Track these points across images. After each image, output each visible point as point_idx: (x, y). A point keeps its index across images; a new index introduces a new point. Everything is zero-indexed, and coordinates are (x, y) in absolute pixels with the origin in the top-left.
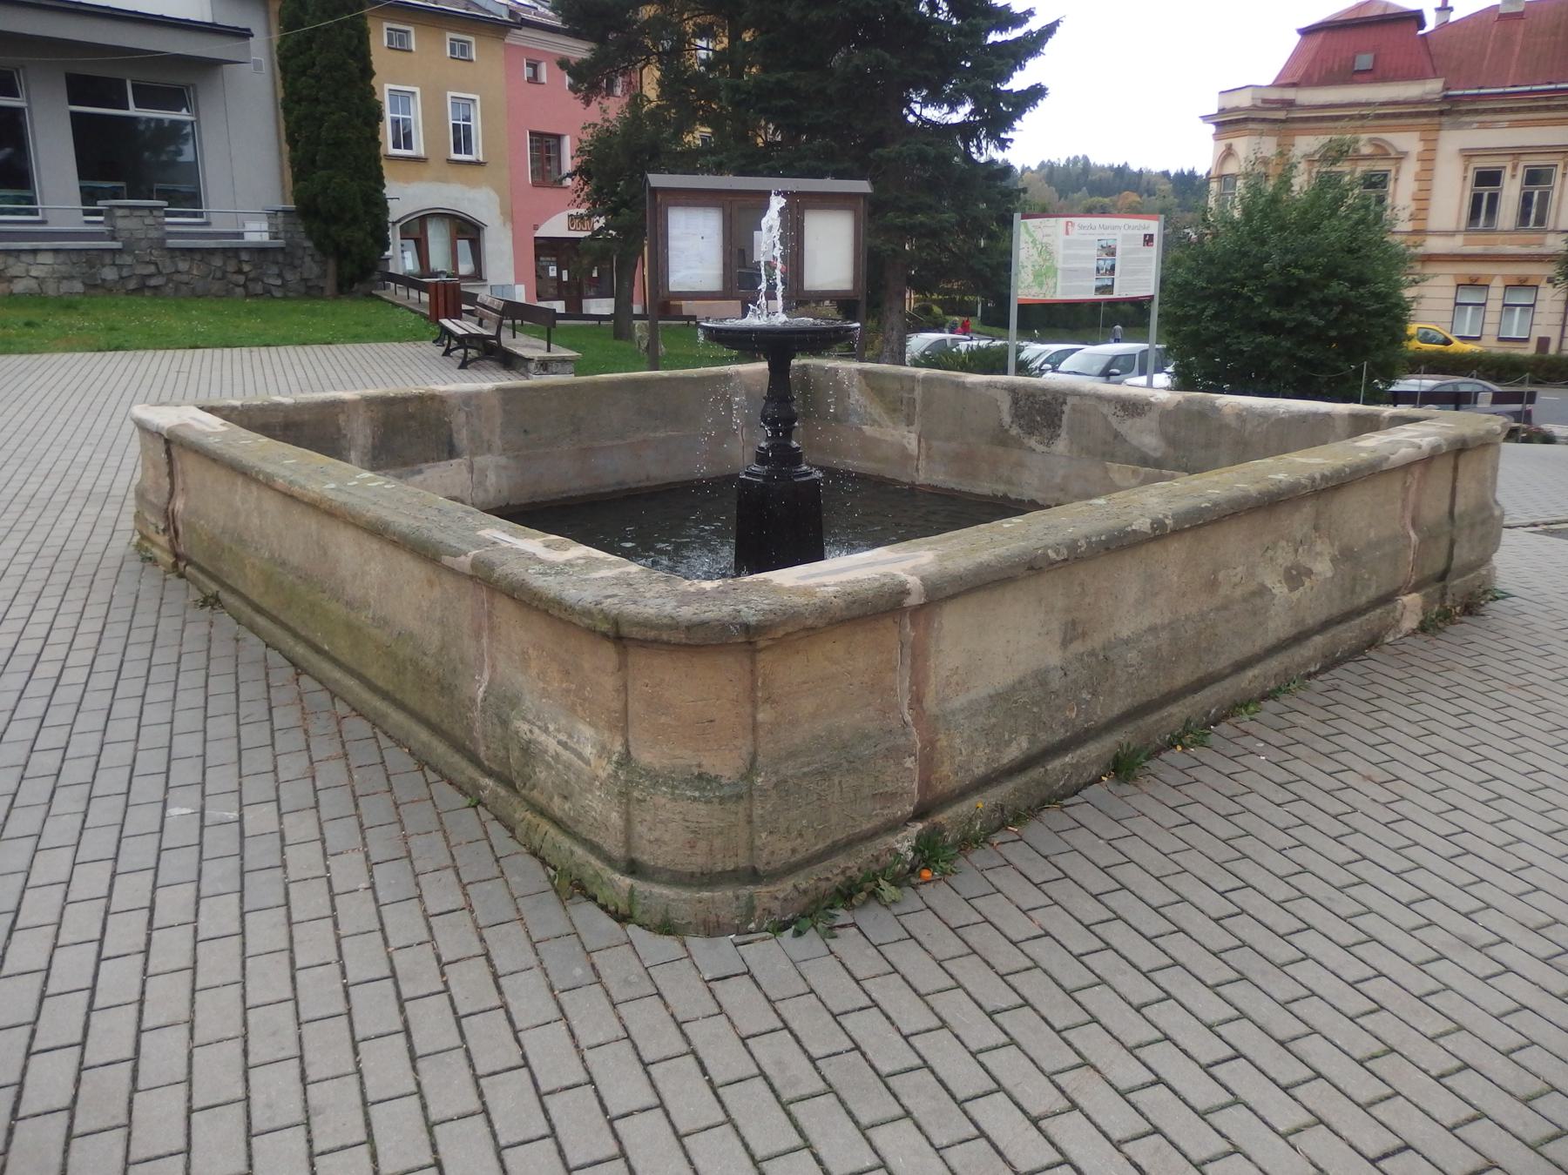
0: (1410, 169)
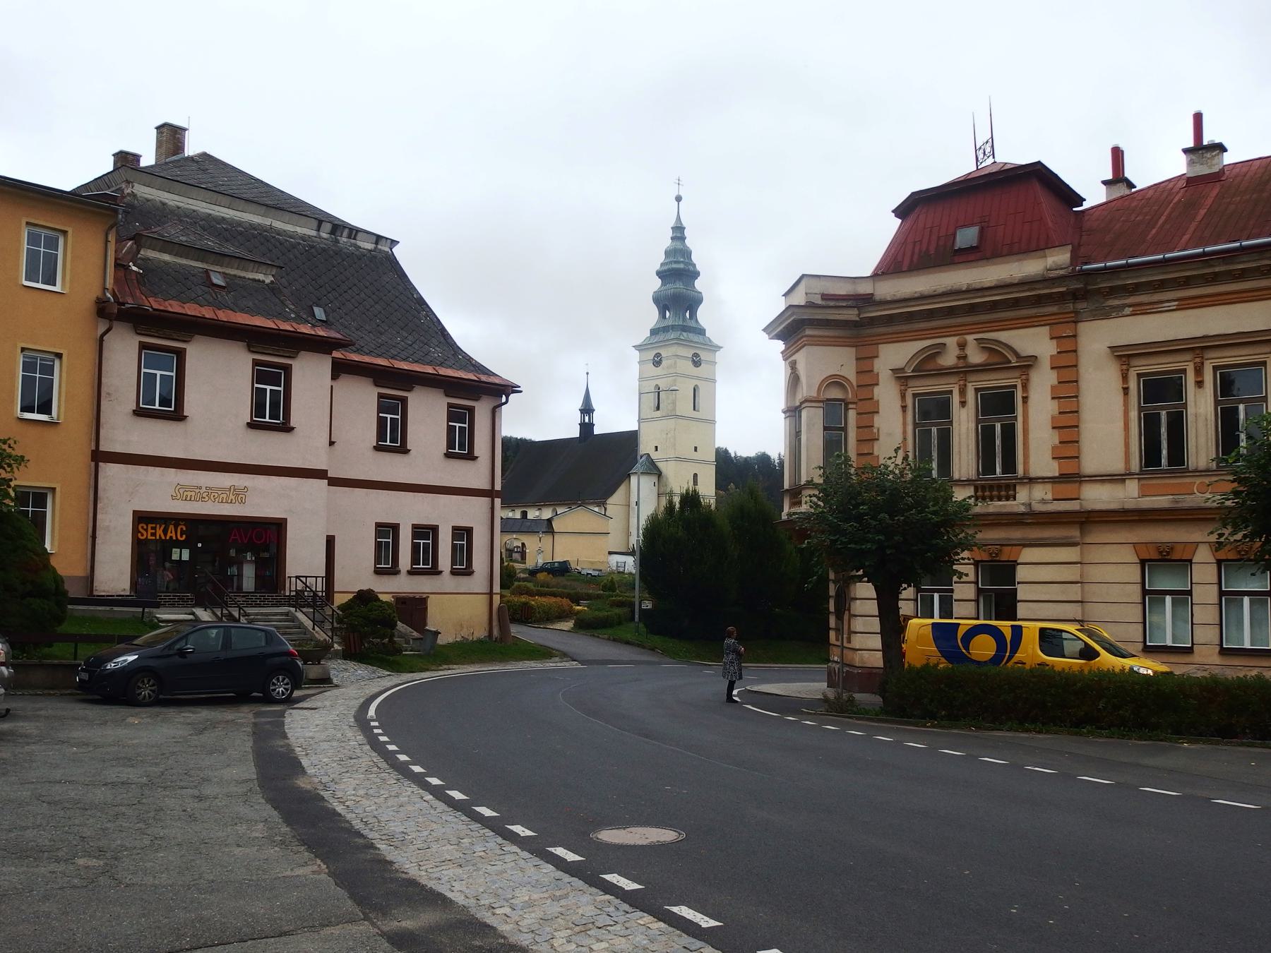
0: (1043, 382)
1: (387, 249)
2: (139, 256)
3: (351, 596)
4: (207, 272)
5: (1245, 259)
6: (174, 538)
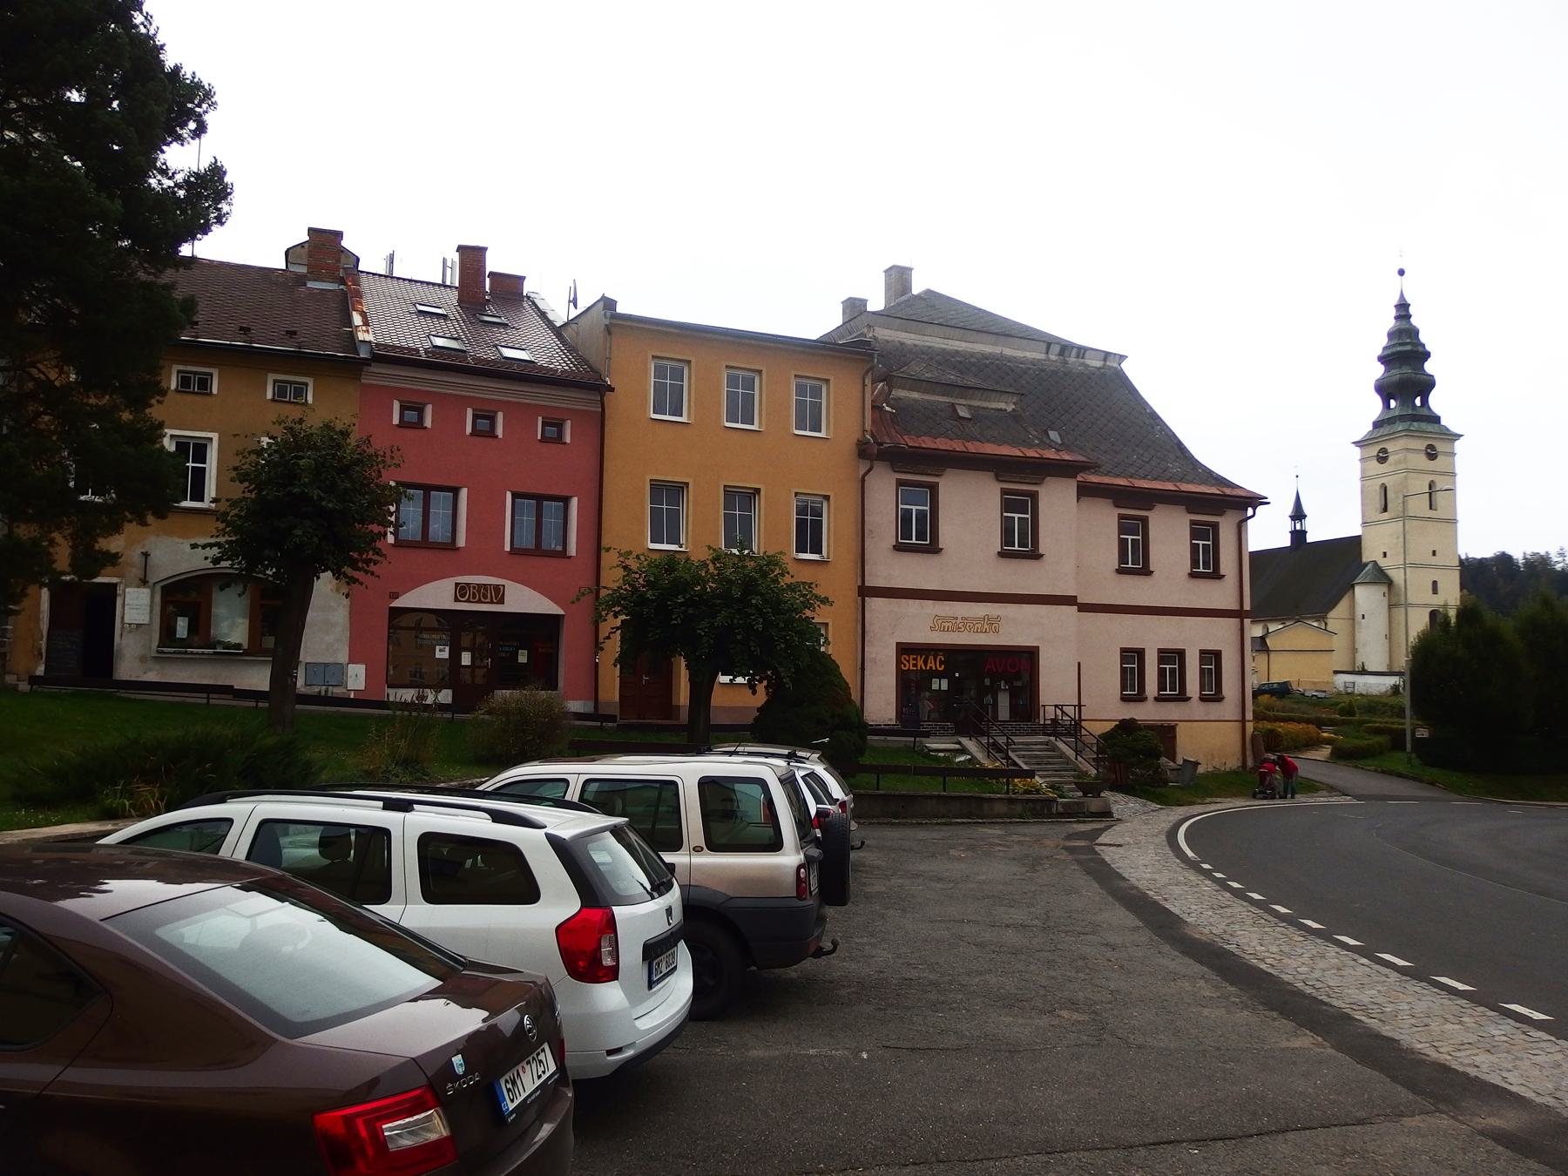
1: (1116, 365)
2: (891, 396)
3: (1109, 726)
4: (953, 405)
6: (934, 668)
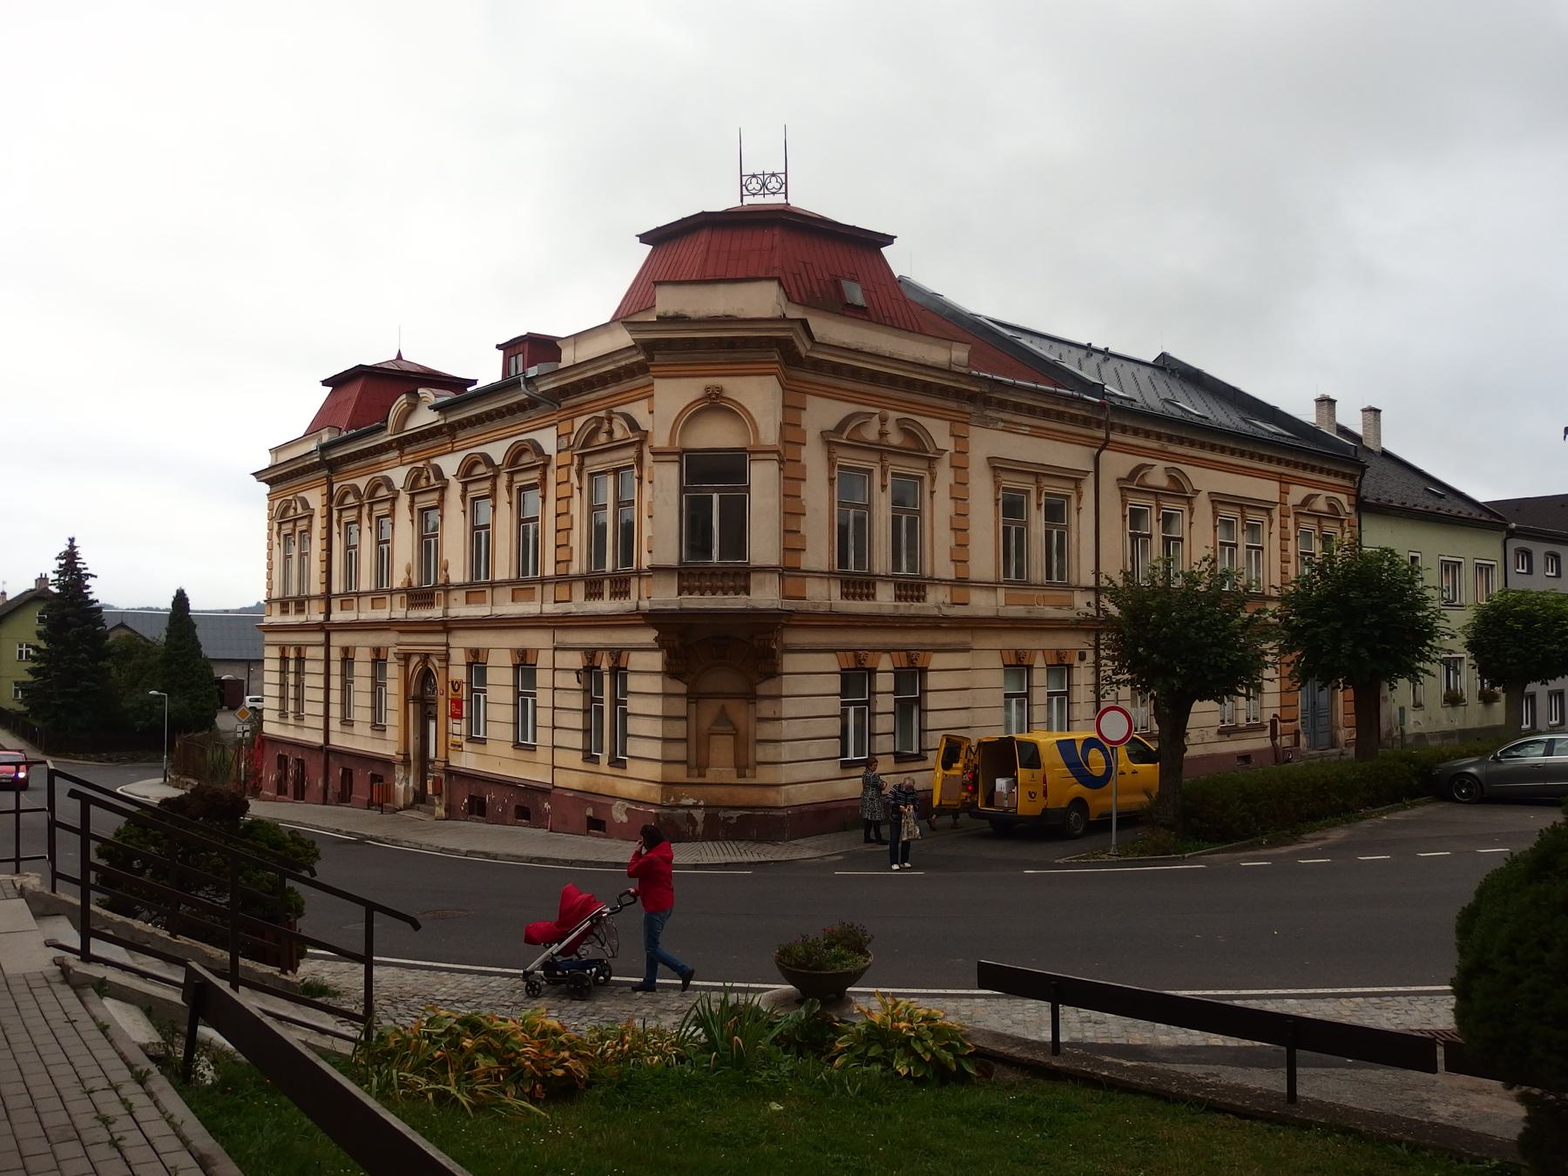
5: (1077, 406)
